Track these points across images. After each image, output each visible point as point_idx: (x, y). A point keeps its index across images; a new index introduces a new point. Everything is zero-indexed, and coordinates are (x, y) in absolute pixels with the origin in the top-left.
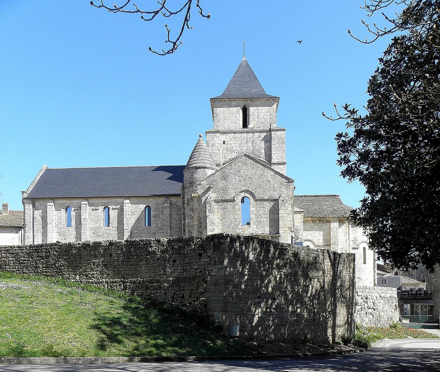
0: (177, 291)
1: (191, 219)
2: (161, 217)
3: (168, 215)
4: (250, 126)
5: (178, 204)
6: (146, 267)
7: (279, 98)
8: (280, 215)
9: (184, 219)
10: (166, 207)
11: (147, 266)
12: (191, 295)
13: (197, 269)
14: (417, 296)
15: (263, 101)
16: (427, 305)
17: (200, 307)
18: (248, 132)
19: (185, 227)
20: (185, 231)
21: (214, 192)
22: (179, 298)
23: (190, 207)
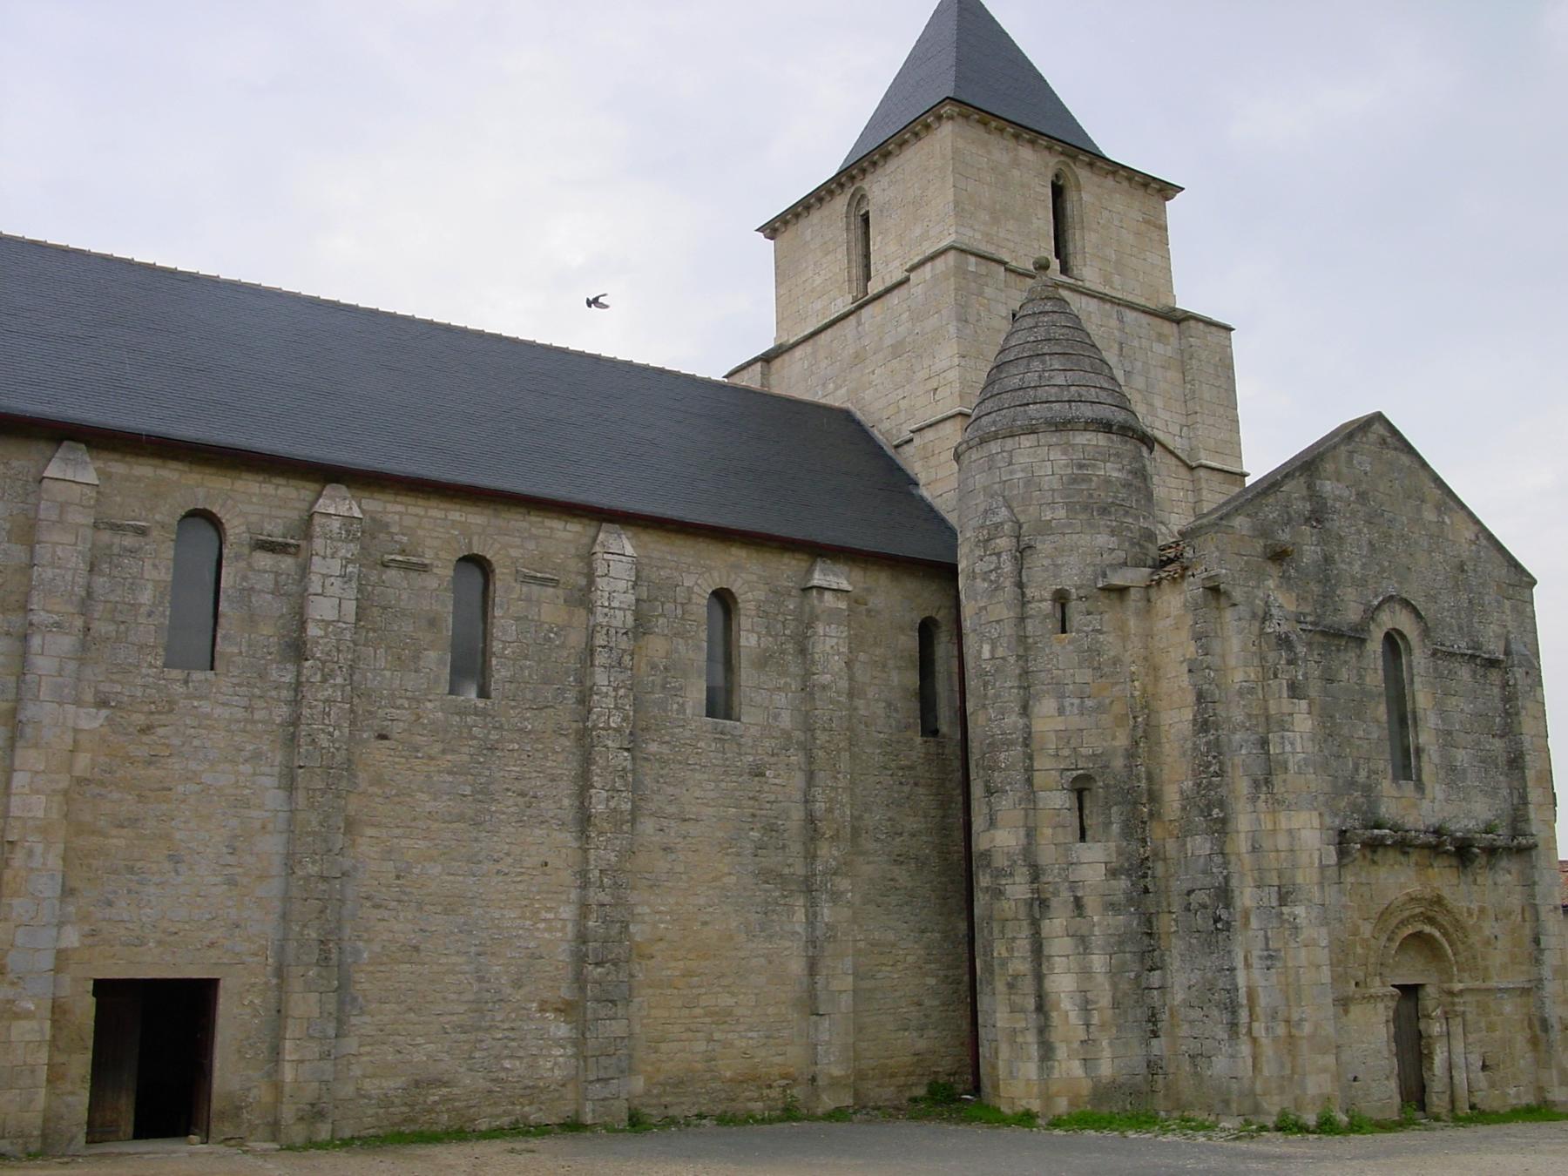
10: (833, 615)
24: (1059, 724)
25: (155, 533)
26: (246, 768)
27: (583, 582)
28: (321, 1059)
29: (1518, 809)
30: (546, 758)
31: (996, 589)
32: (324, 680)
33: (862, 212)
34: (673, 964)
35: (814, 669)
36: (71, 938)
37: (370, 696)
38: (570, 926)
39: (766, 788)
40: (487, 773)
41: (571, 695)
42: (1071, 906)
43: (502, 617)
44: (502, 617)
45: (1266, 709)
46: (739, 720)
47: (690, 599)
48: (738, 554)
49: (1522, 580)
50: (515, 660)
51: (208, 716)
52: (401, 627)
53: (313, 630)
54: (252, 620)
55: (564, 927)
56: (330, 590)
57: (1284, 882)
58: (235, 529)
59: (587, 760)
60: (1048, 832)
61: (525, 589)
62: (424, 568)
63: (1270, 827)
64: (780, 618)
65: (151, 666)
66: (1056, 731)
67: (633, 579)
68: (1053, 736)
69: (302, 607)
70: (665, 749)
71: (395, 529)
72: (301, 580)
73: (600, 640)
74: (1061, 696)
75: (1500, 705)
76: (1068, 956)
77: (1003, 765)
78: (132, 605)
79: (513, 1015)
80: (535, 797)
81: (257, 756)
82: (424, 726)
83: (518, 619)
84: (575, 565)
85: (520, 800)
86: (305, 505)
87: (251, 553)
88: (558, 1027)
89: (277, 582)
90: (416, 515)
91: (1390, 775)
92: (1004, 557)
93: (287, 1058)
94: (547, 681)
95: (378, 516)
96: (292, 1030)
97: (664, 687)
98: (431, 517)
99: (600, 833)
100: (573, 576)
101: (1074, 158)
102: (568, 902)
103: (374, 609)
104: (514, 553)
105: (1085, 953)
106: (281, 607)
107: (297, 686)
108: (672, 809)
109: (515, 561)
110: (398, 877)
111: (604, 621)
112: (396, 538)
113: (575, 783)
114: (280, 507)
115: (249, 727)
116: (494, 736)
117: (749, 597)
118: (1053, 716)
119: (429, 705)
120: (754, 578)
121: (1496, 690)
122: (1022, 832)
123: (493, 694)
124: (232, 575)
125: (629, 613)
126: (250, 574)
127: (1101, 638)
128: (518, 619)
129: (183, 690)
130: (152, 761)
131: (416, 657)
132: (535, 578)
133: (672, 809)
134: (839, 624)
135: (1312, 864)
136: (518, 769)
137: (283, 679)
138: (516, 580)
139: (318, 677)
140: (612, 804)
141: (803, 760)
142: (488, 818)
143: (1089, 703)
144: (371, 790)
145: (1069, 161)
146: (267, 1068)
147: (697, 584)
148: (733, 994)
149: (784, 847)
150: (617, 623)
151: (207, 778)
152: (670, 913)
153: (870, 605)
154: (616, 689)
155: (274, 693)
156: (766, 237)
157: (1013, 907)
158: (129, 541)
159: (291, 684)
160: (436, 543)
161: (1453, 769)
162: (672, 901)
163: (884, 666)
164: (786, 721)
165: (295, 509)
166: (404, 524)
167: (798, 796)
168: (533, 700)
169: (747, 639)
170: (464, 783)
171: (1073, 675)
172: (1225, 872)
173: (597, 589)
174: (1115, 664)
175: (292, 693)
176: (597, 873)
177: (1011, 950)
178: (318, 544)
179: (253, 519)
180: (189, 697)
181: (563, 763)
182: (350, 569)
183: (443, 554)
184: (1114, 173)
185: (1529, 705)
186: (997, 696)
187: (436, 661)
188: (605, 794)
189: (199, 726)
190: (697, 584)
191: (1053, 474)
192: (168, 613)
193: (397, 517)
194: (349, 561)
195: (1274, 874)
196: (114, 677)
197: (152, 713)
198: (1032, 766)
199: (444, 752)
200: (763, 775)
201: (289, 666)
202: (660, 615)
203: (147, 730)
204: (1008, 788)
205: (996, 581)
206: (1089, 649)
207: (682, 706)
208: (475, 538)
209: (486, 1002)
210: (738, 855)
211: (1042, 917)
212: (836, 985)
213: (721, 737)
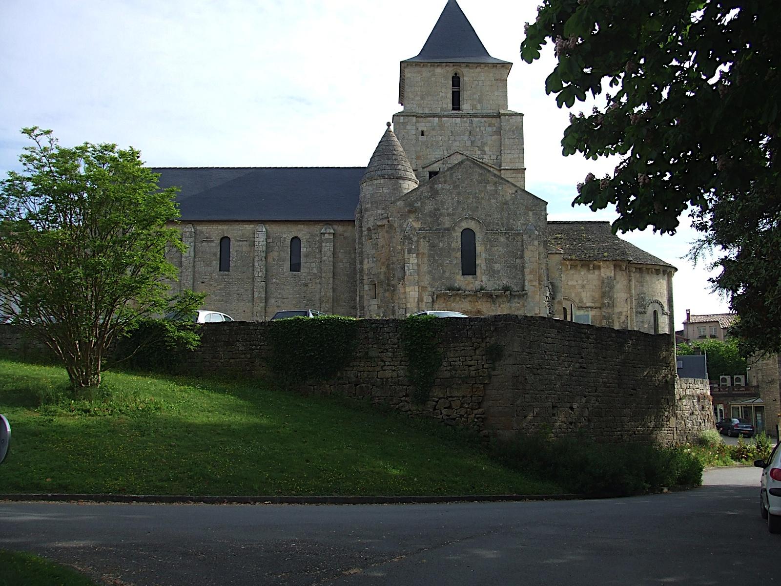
0: (440, 398)
2: (318, 256)
3: (329, 254)
4: (466, 107)
5: (346, 234)
6: (393, 360)
7: (512, 64)
8: (527, 259)
9: (361, 263)
10: (327, 240)
11: (394, 359)
12: (462, 404)
13: (471, 366)
14: (734, 390)
15: (486, 68)
16: (751, 407)
17: (476, 422)
18: (462, 117)
19: (363, 276)
20: (362, 283)
21: (417, 219)
22: (445, 408)
23: (372, 242)
30: (244, 285)
32: (186, 271)
47: (285, 241)
48: (301, 227)
53: (183, 259)
60: (365, 296)
62: (212, 241)
64: (314, 242)
67: (265, 237)
85: (238, 296)
101: (460, 66)
109: (235, 236)
111: (257, 249)
116: (231, 280)
119: (214, 274)
120: (305, 232)
123: (230, 270)
127: (379, 240)
131: (211, 263)
132: (240, 240)
139: (185, 270)
140: (259, 295)
143: (374, 259)
145: (458, 67)
149: (314, 305)
153: (345, 236)
160: (216, 235)
161: (494, 271)
164: (315, 271)
169: (303, 250)
170: (224, 292)
172: (393, 305)
174: (382, 248)
176: (255, 313)
182: (191, 244)
183: (217, 238)
187: (216, 264)
188: (257, 293)
194: (191, 242)
199: (218, 285)
200: (307, 286)
206: (375, 244)
213: (294, 277)
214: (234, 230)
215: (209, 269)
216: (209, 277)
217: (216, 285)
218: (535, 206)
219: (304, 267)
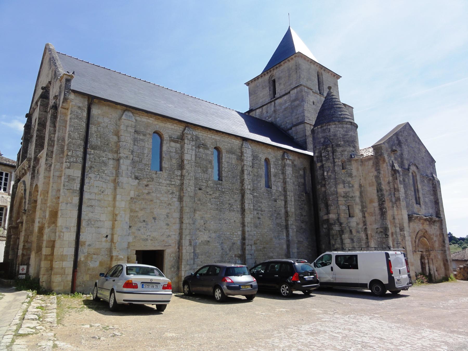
1: (349, 187)
24: (344, 190)
25: (148, 136)
26: (170, 196)
27: (240, 154)
28: (190, 270)
29: (437, 212)
31: (328, 159)
32: (188, 175)
33: (273, 79)
34: (261, 246)
35: (286, 177)
36: (131, 239)
37: (197, 179)
38: (240, 236)
39: (277, 204)
40: (222, 199)
41: (239, 181)
42: (349, 232)
43: (224, 162)
44: (224, 162)
45: (394, 187)
46: (271, 188)
49: (433, 161)
50: (227, 172)
51: (161, 183)
52: (203, 163)
53: (186, 162)
54: (171, 158)
55: (239, 237)
56: (189, 153)
57: (401, 226)
58: (166, 137)
59: (243, 196)
60: (343, 215)
61: (229, 155)
63: (397, 214)
64: (278, 165)
65: (148, 169)
66: (343, 192)
68: (343, 193)
69: (182, 157)
70: (258, 195)
71: (201, 139)
72: (182, 149)
73: (245, 168)
74: (344, 184)
75: (432, 189)
76: (349, 243)
77: (331, 199)
78: (143, 153)
79: (229, 258)
80: (232, 205)
81: (173, 193)
82: (209, 187)
83: (227, 162)
84: (238, 151)
86: (181, 132)
87: (170, 143)
88: (239, 261)
89: (176, 150)
90: (205, 136)
91: (415, 203)
92: (330, 152)
93: (182, 270)
94: (234, 177)
95: (197, 136)
96: (184, 263)
97: (257, 180)
98: (208, 137)
99: (247, 214)
100: (238, 153)
102: (240, 230)
103: (197, 158)
104: (226, 147)
105: (353, 243)
106: (177, 156)
107: (182, 176)
108: (259, 209)
109: (226, 148)
110: (204, 224)
112: (201, 141)
113: (240, 202)
114: (176, 132)
115: (171, 186)
117: (272, 161)
118: (342, 188)
121: (431, 185)
122: (337, 215)
123: (223, 180)
124: (166, 147)
125: (251, 162)
126: (170, 148)
128: (227, 162)
129: (155, 176)
130: (149, 193)
131: (207, 170)
133: (259, 209)
134: (290, 167)
135: (406, 222)
136: (228, 198)
137: (178, 174)
138: (227, 153)
140: (249, 207)
141: (284, 198)
142: (223, 210)
144: (198, 202)
146: (176, 273)
147: (262, 157)
148: (273, 253)
150: (248, 164)
151: (162, 199)
152: (260, 233)
154: (249, 180)
155: (176, 177)
156: (247, 85)
157: (336, 232)
158: (141, 137)
159: (180, 175)
162: (260, 230)
163: (298, 177)
164: (280, 189)
165: (179, 132)
166: (203, 138)
167: (283, 206)
168: (231, 182)
171: (347, 179)
173: (244, 156)
175: (180, 178)
176: (247, 223)
177: (335, 242)
178: (186, 141)
179: (170, 134)
180: (156, 178)
181: (238, 197)
183: (211, 146)
184: (329, 72)
185: (438, 188)
186: (329, 184)
189: (159, 185)
190: (262, 157)
191: (340, 134)
192: (151, 156)
193: (201, 136)
195: (398, 224)
196: (139, 172)
197: (148, 181)
198: (338, 199)
200: (276, 201)
201: (179, 171)
202: (256, 163)
203: (147, 186)
204: (333, 204)
205: (327, 158)
207: (260, 184)
208: (218, 142)
209: (224, 255)
210: (273, 220)
211: (342, 235)
212: (294, 251)
214: (224, 142)
215: (206, 176)
216: (205, 184)
217: (211, 193)
218: (206, 181)
219: (273, 185)
